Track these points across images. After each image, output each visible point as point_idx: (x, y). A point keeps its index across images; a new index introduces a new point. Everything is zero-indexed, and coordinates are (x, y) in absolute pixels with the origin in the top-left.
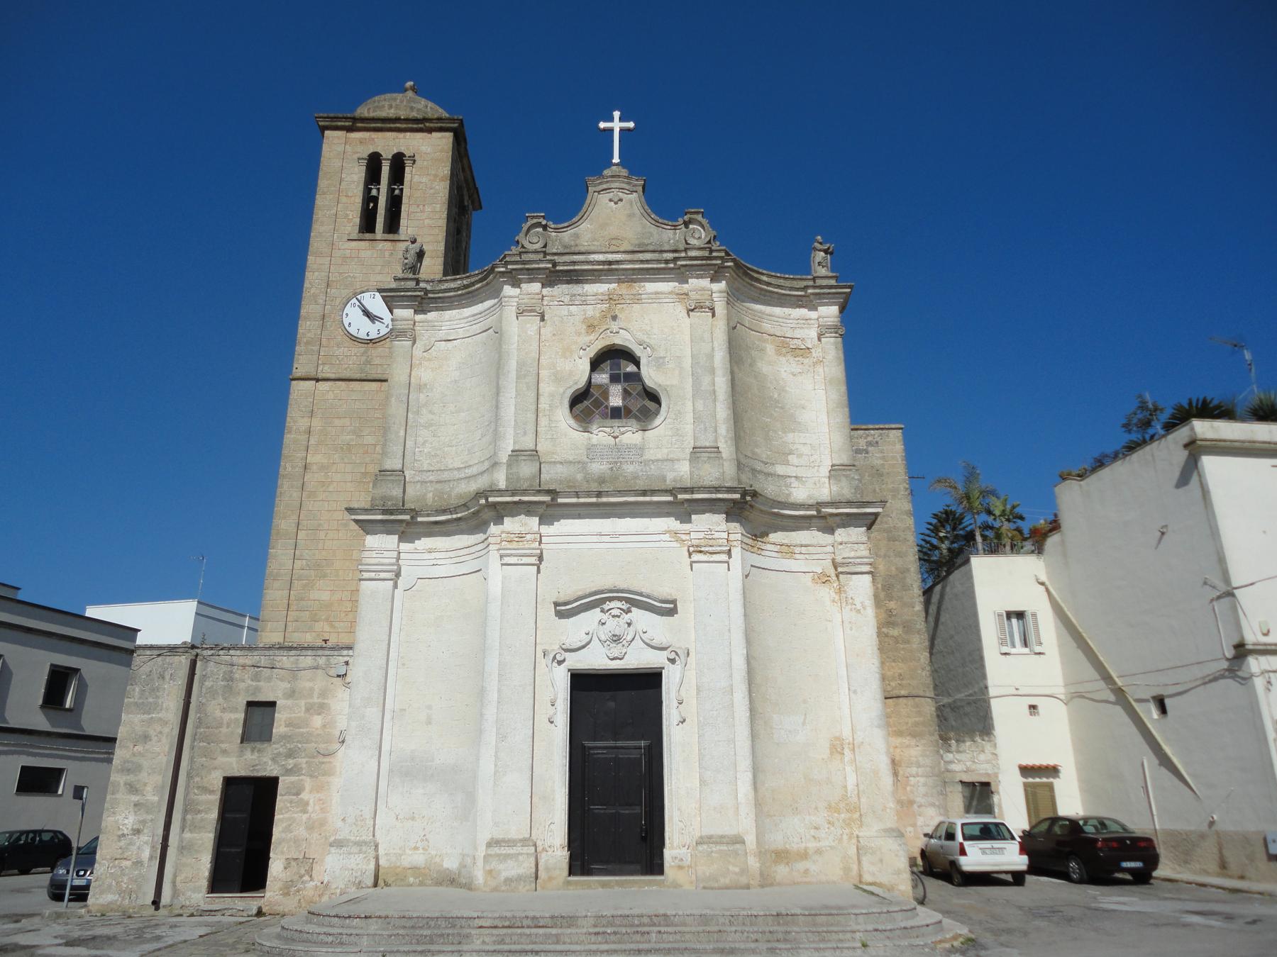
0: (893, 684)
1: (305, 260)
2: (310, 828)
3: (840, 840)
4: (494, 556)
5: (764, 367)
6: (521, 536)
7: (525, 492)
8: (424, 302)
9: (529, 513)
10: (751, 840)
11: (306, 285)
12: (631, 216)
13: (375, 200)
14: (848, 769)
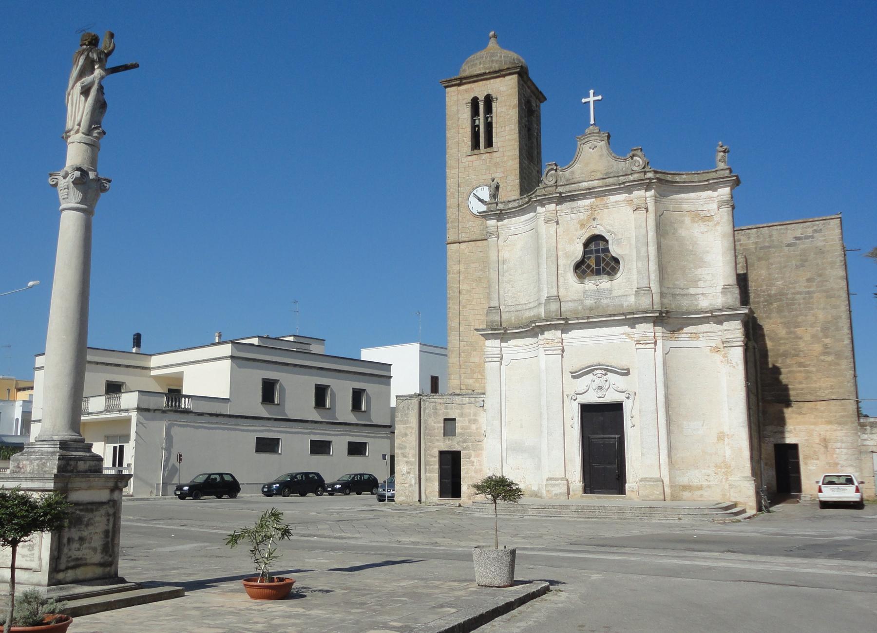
0: (826, 392)
1: (445, 172)
2: (476, 472)
3: (721, 482)
4: (542, 350)
5: (683, 232)
6: (553, 340)
7: (552, 320)
8: (500, 216)
9: (556, 329)
10: (666, 481)
11: (448, 187)
12: (601, 156)
13: (478, 126)
14: (727, 448)
